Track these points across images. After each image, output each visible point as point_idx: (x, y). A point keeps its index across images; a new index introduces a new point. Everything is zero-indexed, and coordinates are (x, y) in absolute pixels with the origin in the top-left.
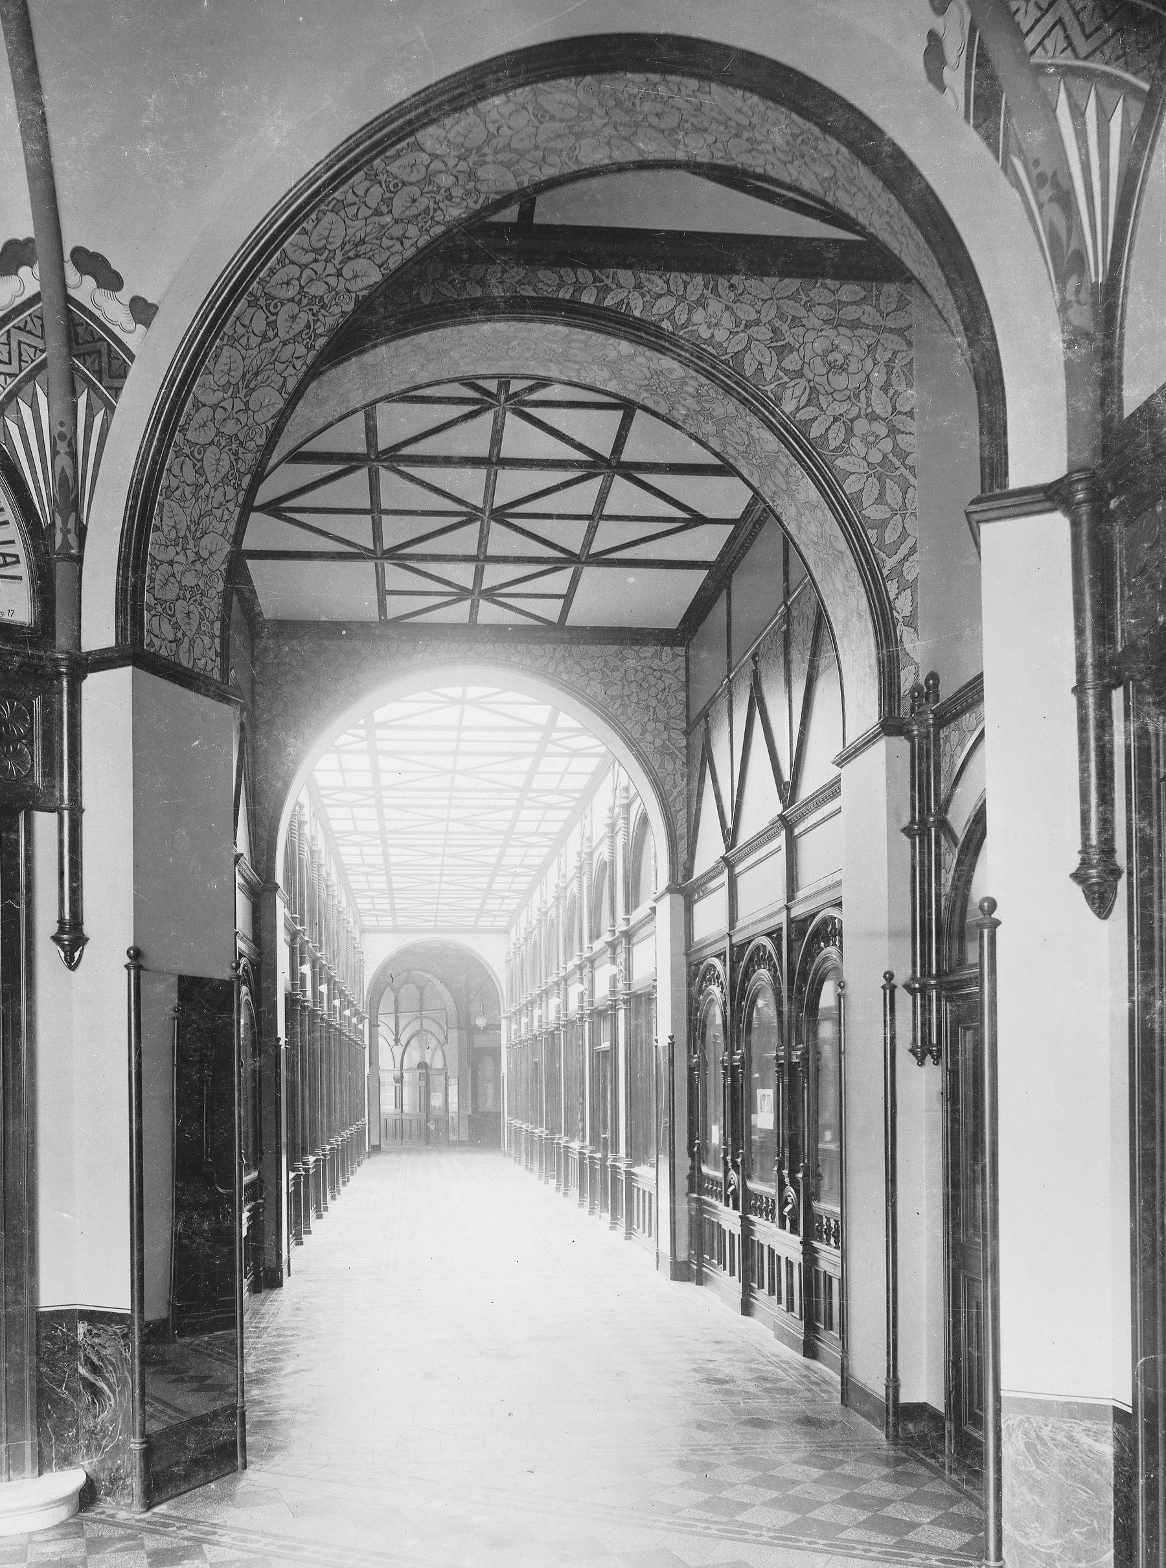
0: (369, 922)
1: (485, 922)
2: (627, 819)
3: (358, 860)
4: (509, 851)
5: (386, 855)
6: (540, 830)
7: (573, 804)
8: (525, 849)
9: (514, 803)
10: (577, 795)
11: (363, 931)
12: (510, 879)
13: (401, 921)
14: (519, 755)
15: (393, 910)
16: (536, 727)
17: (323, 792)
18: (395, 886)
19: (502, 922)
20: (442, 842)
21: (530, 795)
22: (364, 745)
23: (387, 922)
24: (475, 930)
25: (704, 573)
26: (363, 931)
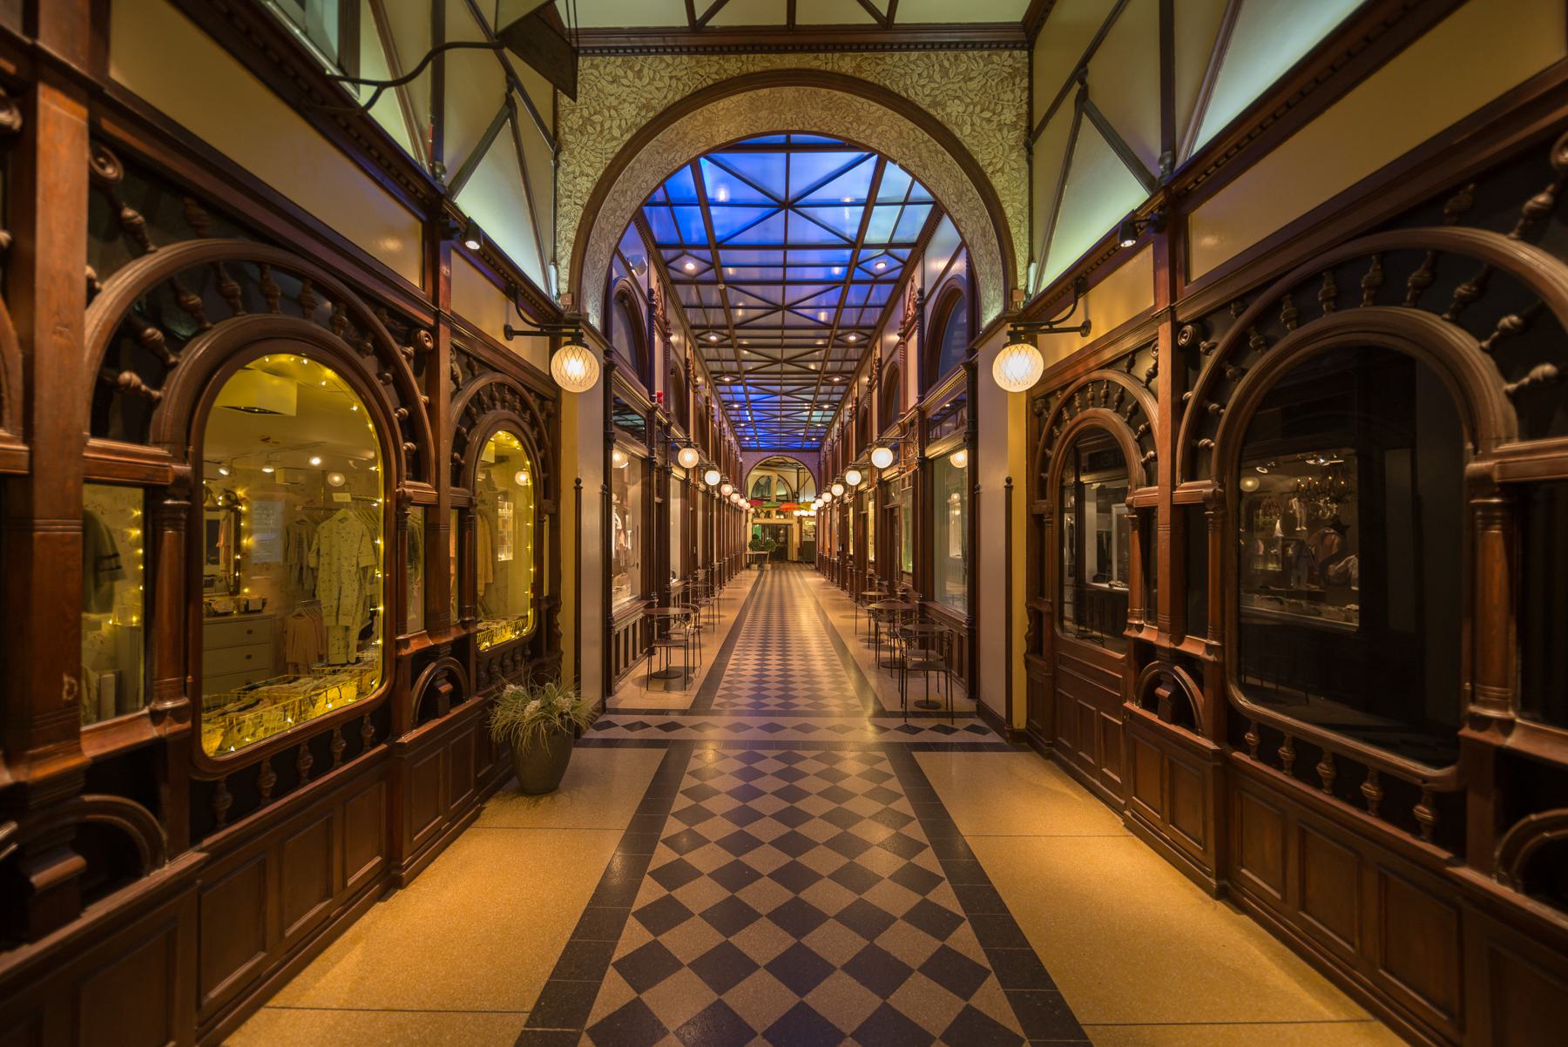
6: (862, 322)
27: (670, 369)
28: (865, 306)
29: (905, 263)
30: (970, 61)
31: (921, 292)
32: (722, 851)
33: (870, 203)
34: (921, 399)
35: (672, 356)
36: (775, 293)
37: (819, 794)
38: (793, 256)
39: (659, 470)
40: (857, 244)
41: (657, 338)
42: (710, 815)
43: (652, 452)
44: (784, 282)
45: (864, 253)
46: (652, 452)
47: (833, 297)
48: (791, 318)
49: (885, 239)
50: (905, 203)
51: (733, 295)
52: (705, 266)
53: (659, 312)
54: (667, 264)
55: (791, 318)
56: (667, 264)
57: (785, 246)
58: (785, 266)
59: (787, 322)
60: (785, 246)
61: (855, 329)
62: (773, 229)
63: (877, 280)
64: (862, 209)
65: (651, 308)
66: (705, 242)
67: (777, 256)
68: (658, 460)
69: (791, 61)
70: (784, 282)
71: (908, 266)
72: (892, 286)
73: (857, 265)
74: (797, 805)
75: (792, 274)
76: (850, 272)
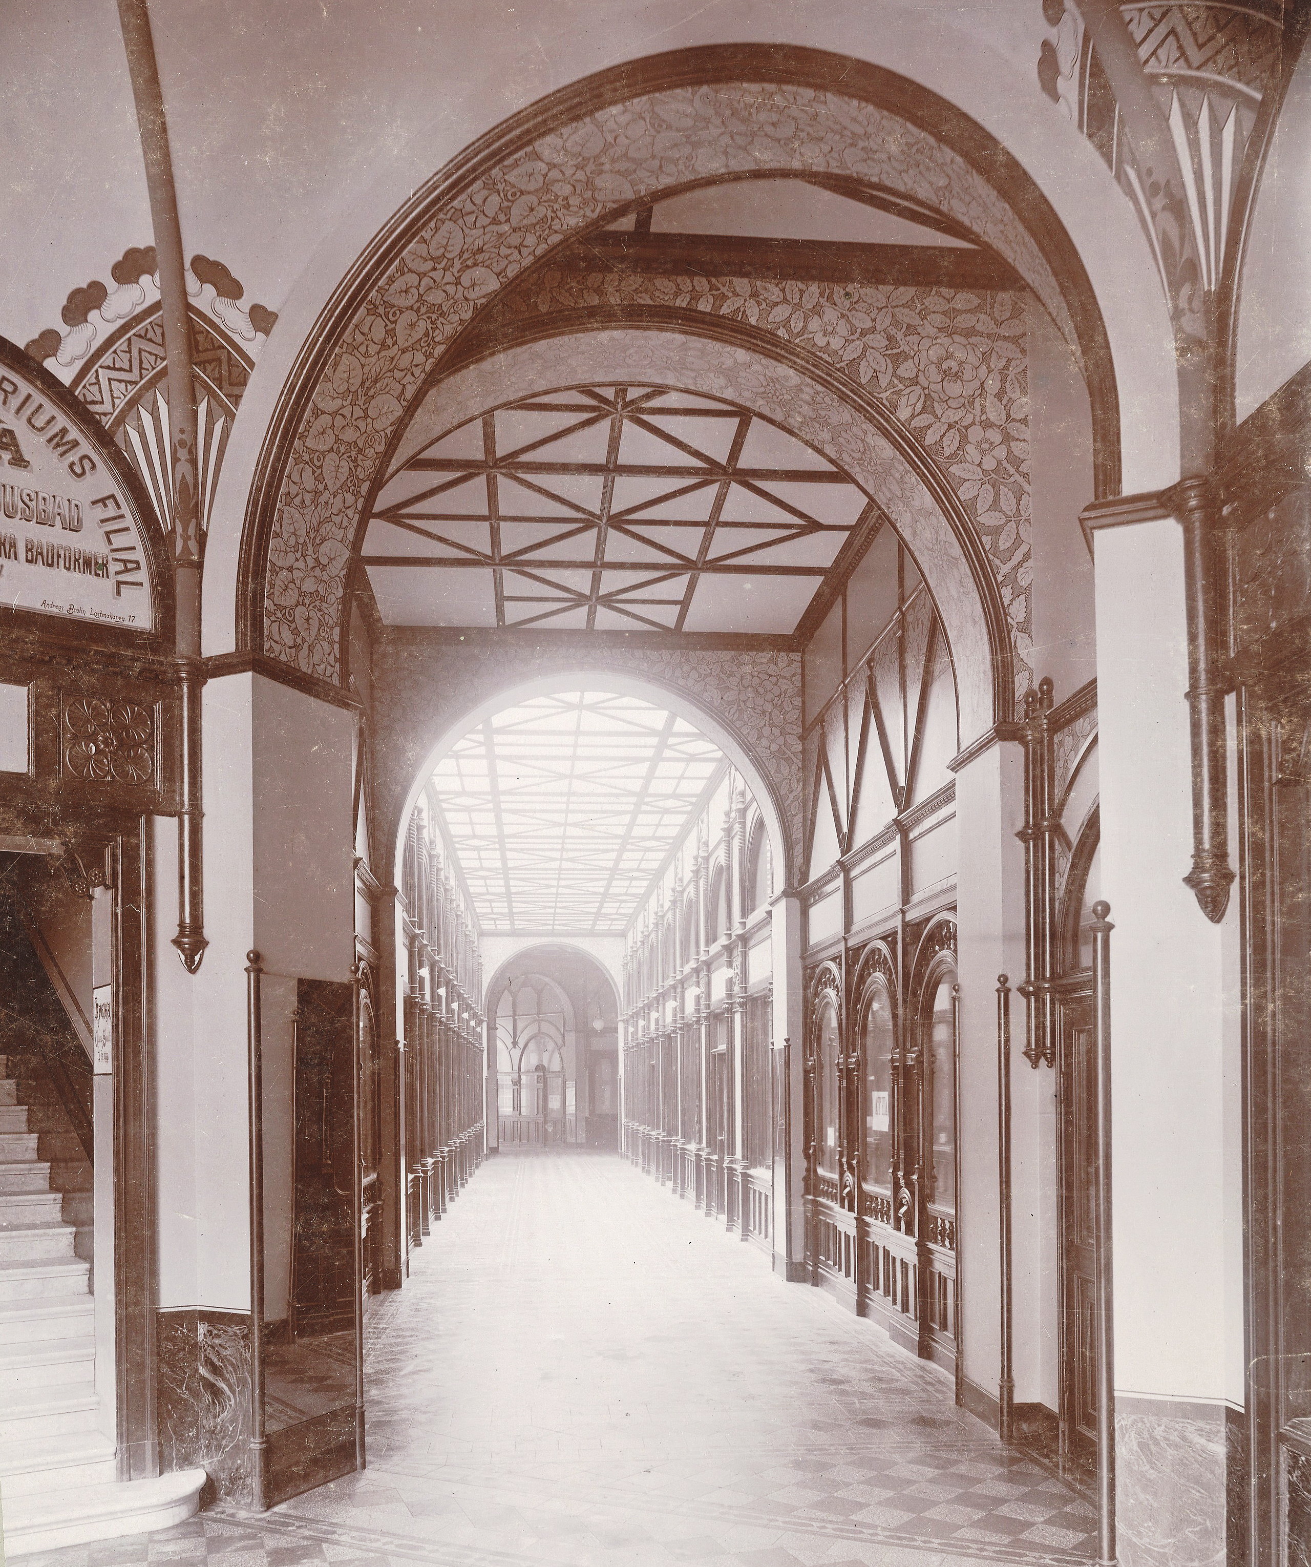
0: (487, 925)
1: (602, 926)
2: (743, 824)
3: (476, 864)
4: (626, 855)
5: (499, 823)
7: (689, 808)
8: (641, 853)
9: (631, 807)
10: (694, 800)
11: (482, 934)
12: (627, 883)
13: (519, 925)
14: (637, 760)
15: (511, 914)
16: (653, 732)
17: (442, 797)
18: (513, 890)
19: (619, 926)
20: (564, 806)
21: (647, 800)
22: (482, 750)
23: (505, 925)
24: (592, 934)
25: (820, 579)
26: (482, 934)
59: (568, 834)
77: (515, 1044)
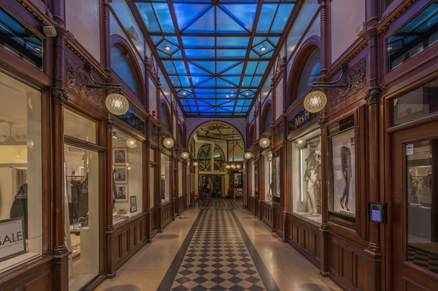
9: (243, 53)
27: (179, 126)
28: (254, 75)
29: (255, 93)
30: (240, 119)
31: (285, 58)
32: (212, 282)
33: (243, 75)
34: (285, 112)
35: (179, 122)
36: (213, 102)
37: (243, 272)
38: (218, 91)
39: (175, 159)
40: (239, 87)
41: (174, 116)
42: (206, 280)
43: (147, 138)
44: (216, 59)
45: (257, 40)
46: (172, 153)
47: (232, 103)
48: (220, 82)
49: (248, 85)
50: (243, 106)
51: (199, 102)
52: (175, 48)
53: (175, 108)
54: (176, 93)
55: (220, 82)
56: (176, 93)
57: (216, 88)
58: (216, 93)
60: (216, 34)
61: (249, 88)
62: (212, 83)
63: (246, 98)
64: (240, 77)
65: (172, 108)
66: (174, 32)
67: (211, 41)
68: (175, 155)
69: (216, 119)
70: (216, 59)
71: (257, 94)
72: (252, 100)
73: (240, 93)
74: (236, 276)
75: (218, 96)
76: (248, 54)
77: (206, 168)
